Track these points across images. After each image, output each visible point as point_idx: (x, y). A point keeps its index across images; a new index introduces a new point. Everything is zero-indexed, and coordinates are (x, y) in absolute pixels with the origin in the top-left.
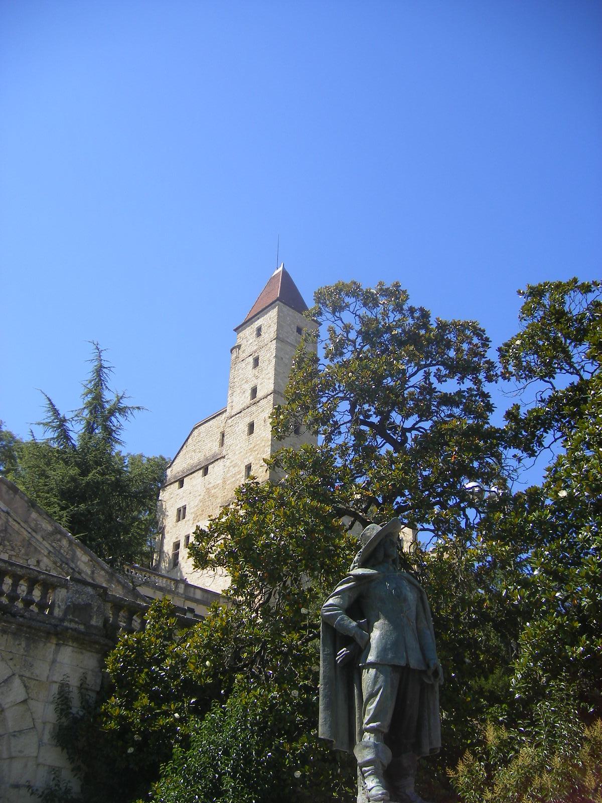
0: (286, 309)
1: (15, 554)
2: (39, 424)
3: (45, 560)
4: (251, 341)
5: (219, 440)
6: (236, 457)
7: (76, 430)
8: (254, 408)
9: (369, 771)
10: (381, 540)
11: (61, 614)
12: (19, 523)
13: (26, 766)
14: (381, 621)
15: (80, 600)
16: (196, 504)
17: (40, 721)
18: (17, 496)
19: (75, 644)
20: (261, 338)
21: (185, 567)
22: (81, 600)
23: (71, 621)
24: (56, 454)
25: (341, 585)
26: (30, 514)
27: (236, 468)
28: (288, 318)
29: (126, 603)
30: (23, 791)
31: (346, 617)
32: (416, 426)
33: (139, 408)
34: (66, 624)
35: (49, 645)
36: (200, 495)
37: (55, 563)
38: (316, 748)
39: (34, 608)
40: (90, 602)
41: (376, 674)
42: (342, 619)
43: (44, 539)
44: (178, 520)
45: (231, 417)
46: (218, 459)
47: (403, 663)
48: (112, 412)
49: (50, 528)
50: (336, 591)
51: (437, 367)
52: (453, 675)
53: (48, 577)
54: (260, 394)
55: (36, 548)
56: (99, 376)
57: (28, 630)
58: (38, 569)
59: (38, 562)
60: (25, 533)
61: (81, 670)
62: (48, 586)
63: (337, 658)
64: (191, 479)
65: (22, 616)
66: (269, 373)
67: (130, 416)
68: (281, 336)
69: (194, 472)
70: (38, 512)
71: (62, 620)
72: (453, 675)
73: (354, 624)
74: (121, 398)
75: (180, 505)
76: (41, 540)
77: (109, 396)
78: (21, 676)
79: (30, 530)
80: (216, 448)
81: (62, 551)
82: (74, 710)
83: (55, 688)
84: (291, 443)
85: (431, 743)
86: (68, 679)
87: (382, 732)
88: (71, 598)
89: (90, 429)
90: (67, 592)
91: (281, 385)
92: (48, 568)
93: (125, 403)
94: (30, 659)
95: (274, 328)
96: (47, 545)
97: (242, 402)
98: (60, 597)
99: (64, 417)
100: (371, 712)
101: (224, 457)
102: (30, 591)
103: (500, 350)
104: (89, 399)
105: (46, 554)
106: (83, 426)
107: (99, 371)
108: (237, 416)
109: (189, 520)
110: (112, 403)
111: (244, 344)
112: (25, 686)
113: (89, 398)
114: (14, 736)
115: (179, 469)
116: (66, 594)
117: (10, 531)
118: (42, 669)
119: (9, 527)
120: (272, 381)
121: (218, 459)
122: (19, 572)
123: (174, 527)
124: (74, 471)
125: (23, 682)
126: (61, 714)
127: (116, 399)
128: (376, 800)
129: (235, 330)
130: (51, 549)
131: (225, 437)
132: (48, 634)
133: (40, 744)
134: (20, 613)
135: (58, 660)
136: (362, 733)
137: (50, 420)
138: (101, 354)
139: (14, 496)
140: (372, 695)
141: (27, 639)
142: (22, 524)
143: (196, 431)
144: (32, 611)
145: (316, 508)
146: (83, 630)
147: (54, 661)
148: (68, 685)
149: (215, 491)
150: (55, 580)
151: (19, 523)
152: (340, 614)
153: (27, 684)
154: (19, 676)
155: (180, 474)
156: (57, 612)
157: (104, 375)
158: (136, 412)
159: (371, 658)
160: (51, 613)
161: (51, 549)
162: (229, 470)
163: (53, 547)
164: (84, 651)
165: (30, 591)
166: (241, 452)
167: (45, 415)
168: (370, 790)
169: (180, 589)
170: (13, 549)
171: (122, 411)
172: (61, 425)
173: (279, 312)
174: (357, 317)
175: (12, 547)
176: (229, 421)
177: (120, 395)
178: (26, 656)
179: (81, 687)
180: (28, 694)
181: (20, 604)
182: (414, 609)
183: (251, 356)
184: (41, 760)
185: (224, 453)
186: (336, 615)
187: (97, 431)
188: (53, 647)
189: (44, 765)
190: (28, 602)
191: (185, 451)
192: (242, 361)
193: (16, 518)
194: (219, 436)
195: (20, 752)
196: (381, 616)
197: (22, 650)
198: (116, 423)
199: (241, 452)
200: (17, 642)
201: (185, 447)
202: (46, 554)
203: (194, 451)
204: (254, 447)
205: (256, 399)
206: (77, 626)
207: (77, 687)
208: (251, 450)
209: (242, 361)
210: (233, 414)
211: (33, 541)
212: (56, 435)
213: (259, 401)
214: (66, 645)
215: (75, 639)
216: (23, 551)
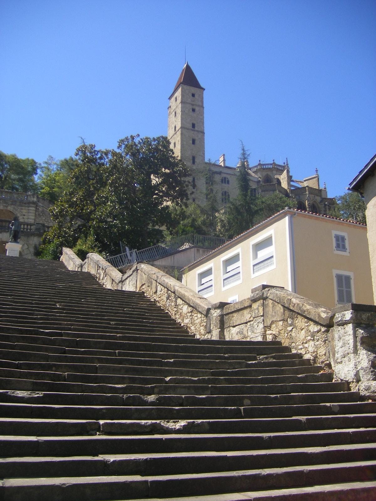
54: (177, 129)
78: (27, 244)
83: (34, 245)
102: (27, 227)
122: (24, 223)
165: (27, 227)
181: (25, 230)
190: (27, 229)
193: (45, 207)
205: (176, 131)
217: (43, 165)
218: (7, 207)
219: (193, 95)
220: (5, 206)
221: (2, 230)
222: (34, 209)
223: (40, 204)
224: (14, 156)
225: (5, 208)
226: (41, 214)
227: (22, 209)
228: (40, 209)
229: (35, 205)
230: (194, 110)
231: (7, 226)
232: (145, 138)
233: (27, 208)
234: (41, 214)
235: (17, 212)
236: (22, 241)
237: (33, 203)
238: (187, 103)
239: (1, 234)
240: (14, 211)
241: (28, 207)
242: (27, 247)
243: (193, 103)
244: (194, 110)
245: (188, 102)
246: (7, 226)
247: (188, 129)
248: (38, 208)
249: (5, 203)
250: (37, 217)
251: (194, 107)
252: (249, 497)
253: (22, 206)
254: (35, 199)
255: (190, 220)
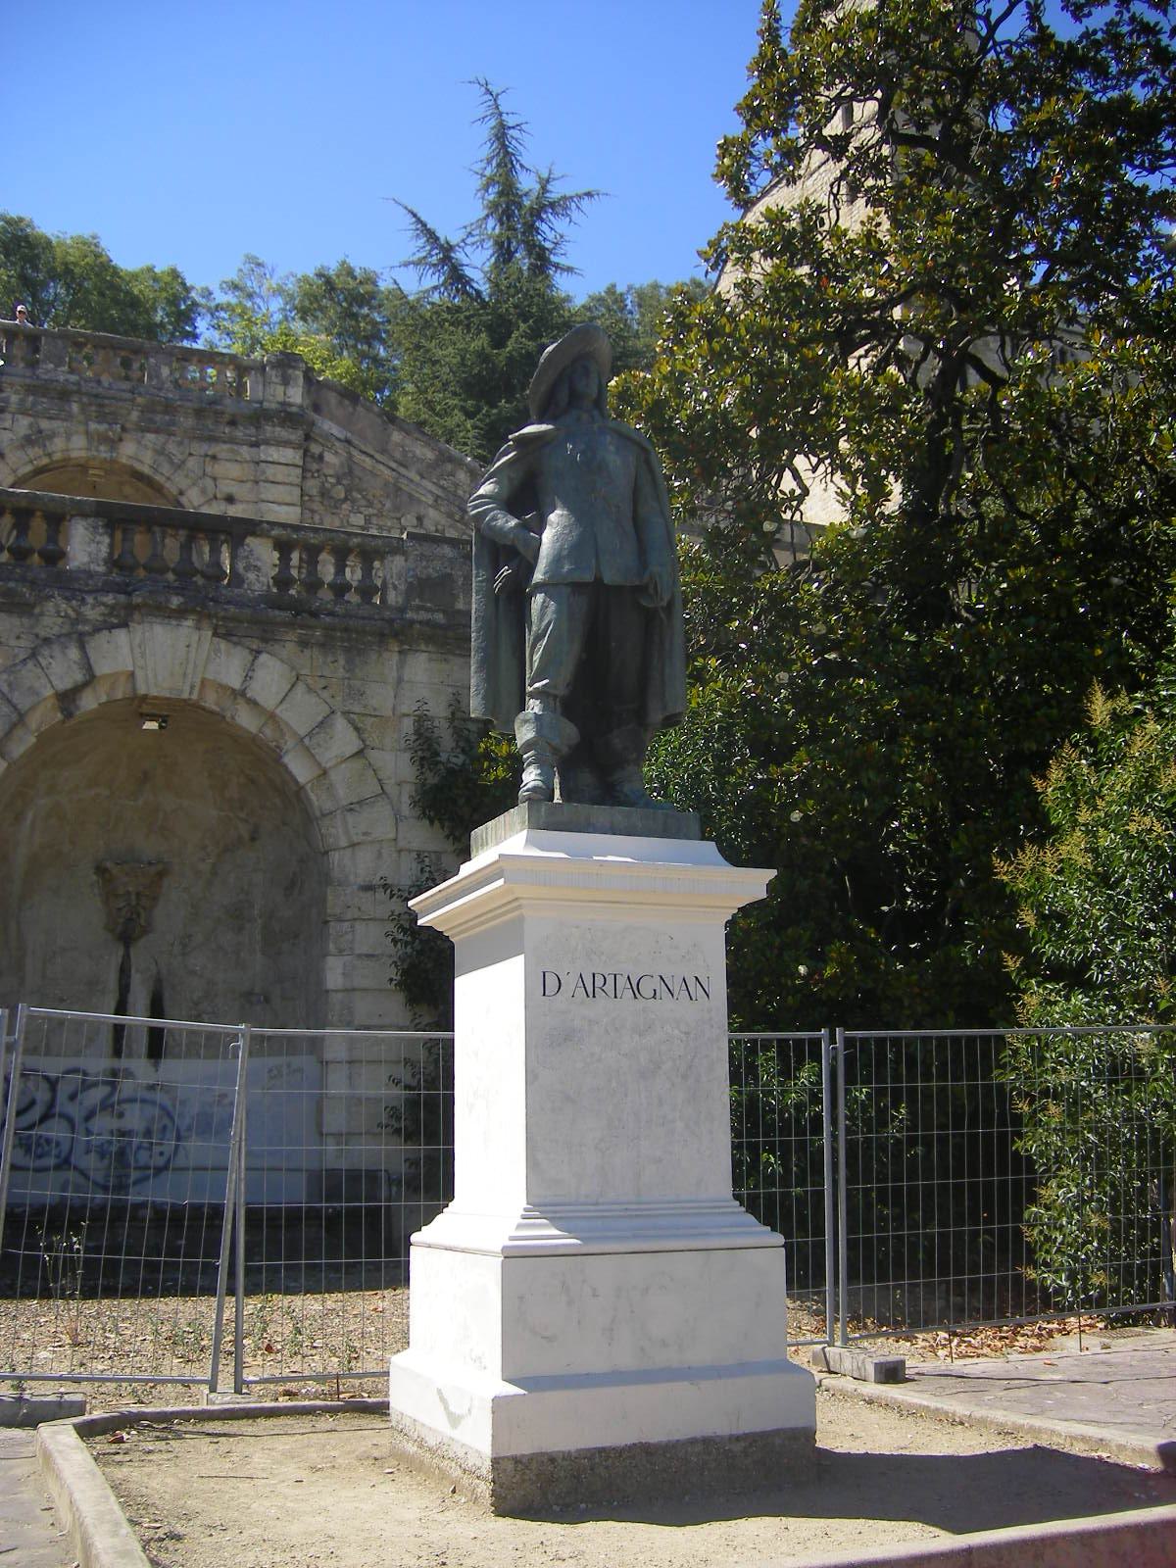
1: (375, 512)
2: (406, 264)
3: (432, 513)
7: (478, 263)
11: (400, 600)
12: (372, 456)
13: (380, 855)
14: (558, 512)
15: (431, 570)
17: (393, 781)
18: (359, 409)
19: (431, 648)
22: (433, 570)
23: (419, 608)
24: (445, 316)
26: (389, 436)
30: (380, 895)
33: (589, 194)
34: (409, 615)
35: (386, 655)
37: (450, 515)
38: (824, 768)
39: (353, 598)
40: (448, 571)
41: (544, 602)
42: (494, 519)
43: (422, 477)
47: (588, 577)
48: (537, 212)
49: (430, 455)
52: (1082, 610)
53: (367, 540)
55: (411, 496)
56: (504, 147)
57: (345, 635)
58: (423, 531)
59: (420, 519)
60: (387, 472)
61: (450, 690)
62: (369, 555)
65: (331, 614)
67: (575, 214)
70: (401, 429)
71: (402, 610)
72: (1082, 610)
73: (513, 522)
74: (548, 181)
76: (417, 478)
77: (527, 183)
78: (346, 713)
79: (394, 465)
81: (460, 492)
82: (443, 757)
83: (408, 725)
86: (425, 707)
88: (414, 570)
89: (504, 253)
90: (406, 560)
92: (440, 527)
93: (556, 191)
94: (357, 683)
96: (434, 489)
98: (392, 570)
99: (447, 243)
102: (340, 569)
104: (491, 197)
105: (430, 502)
106: (490, 252)
107: (501, 134)
108: (823, 168)
110: (534, 195)
112: (357, 729)
113: (492, 194)
114: (351, 810)
116: (403, 563)
117: (357, 472)
118: (380, 698)
119: (354, 467)
122: (314, 539)
124: (483, 340)
125: (351, 722)
126: (422, 766)
127: (538, 187)
130: (439, 492)
132: (382, 638)
133: (398, 818)
134: (326, 609)
135: (406, 678)
137: (424, 254)
138: (499, 102)
139: (355, 409)
141: (347, 650)
142: (378, 456)
144: (349, 602)
145: (772, 330)
146: (443, 621)
147: (400, 680)
148: (431, 719)
150: (380, 542)
151: (372, 456)
152: (492, 509)
153: (360, 725)
154: (343, 713)
156: (393, 598)
157: (514, 142)
158: (585, 203)
159: (538, 576)
160: (383, 600)
161: (439, 492)
163: (442, 487)
164: (451, 657)
165: (340, 569)
167: (413, 246)
170: (370, 505)
171: (560, 206)
172: (445, 256)
175: (368, 501)
177: (545, 175)
178: (349, 679)
179: (452, 718)
180: (363, 741)
181: (326, 595)
184: (402, 844)
186: (485, 513)
187: (518, 255)
188: (395, 657)
189: (410, 851)
193: (363, 448)
195: (365, 834)
196: (558, 503)
197: (342, 670)
198: (550, 235)
200: (330, 659)
202: (430, 502)
206: (430, 616)
207: (446, 718)
211: (403, 484)
212: (442, 279)
214: (417, 651)
215: (429, 639)
216: (388, 505)
217: (221, 298)
218: (114, 443)
220: (104, 439)
221: (137, 599)
222: (291, 455)
223: (328, 426)
224: (90, 249)
225: (104, 452)
226: (340, 492)
227: (214, 458)
228: (329, 457)
229: (300, 433)
231: (142, 560)
233: (245, 452)
234: (340, 492)
235: (180, 481)
236: (310, 690)
237: (287, 417)
239: (2, 615)
240: (166, 469)
241: (256, 445)
242: (352, 744)
246: (142, 560)
248: (315, 449)
249: (101, 418)
250: (313, 511)
253: (213, 439)
254: (296, 395)
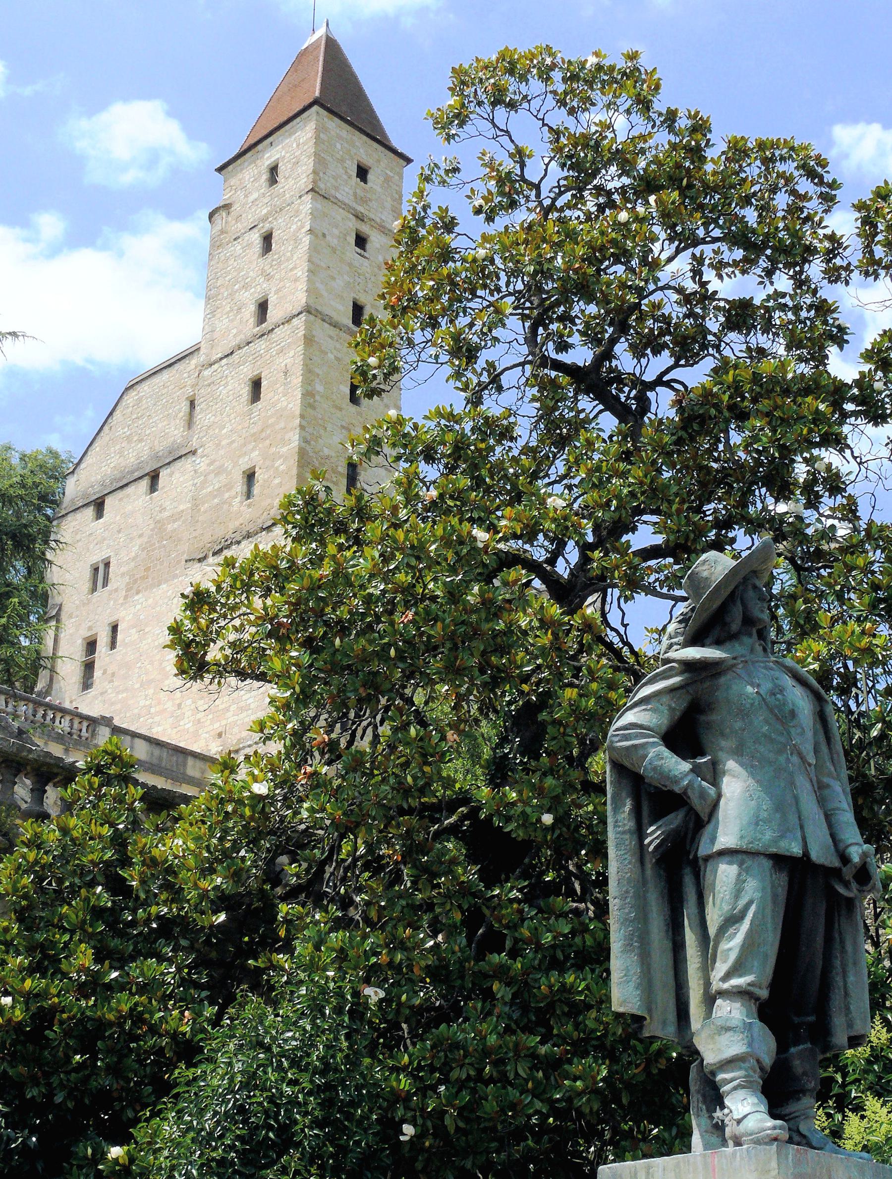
0: (334, 125)
4: (255, 195)
5: (182, 414)
6: (222, 452)
8: (261, 345)
9: (732, 1080)
10: (736, 587)
16: (133, 554)
20: (278, 188)
21: (110, 691)
25: (652, 681)
27: (223, 477)
28: (339, 146)
29: (31, 756)
31: (666, 752)
32: (665, 379)
33: (14, 334)
36: (141, 536)
41: (739, 875)
42: (659, 756)
44: (94, 589)
45: (211, 365)
46: (180, 457)
47: (796, 850)
50: (636, 699)
51: (715, 246)
54: (274, 314)
63: (646, 841)
64: (121, 500)
66: (295, 268)
68: (322, 186)
69: (126, 485)
75: (97, 557)
80: (176, 432)
84: (344, 424)
85: (850, 1025)
87: (757, 999)
91: (321, 296)
95: (307, 165)
97: (234, 331)
100: (733, 956)
101: (193, 453)
103: (860, 207)
108: (224, 361)
109: (116, 590)
111: (239, 200)
115: (93, 479)
120: (302, 286)
121: (180, 457)
123: (84, 604)
128: (758, 1142)
129: (220, 170)
131: (198, 408)
136: (710, 1000)
140: (732, 920)
143: (132, 393)
149: (176, 525)
155: (97, 488)
162: (204, 482)
166: (233, 442)
168: (739, 1122)
169: (100, 738)
173: (318, 131)
174: (546, 128)
176: (206, 373)
182: (809, 734)
183: (255, 230)
185: (194, 443)
191: (107, 438)
192: (235, 239)
194: (185, 406)
199: (233, 442)
201: (106, 428)
203: (129, 439)
204: (262, 430)
208: (256, 438)
209: (235, 239)
210: (215, 358)
213: (273, 329)
219: (362, 173)
230: (361, 241)
232: (212, 644)
238: (337, 202)
243: (360, 209)
244: (361, 241)
245: (338, 195)
247: (335, 325)
251: (365, 229)
252: (644, 883)
255: (621, 109)
